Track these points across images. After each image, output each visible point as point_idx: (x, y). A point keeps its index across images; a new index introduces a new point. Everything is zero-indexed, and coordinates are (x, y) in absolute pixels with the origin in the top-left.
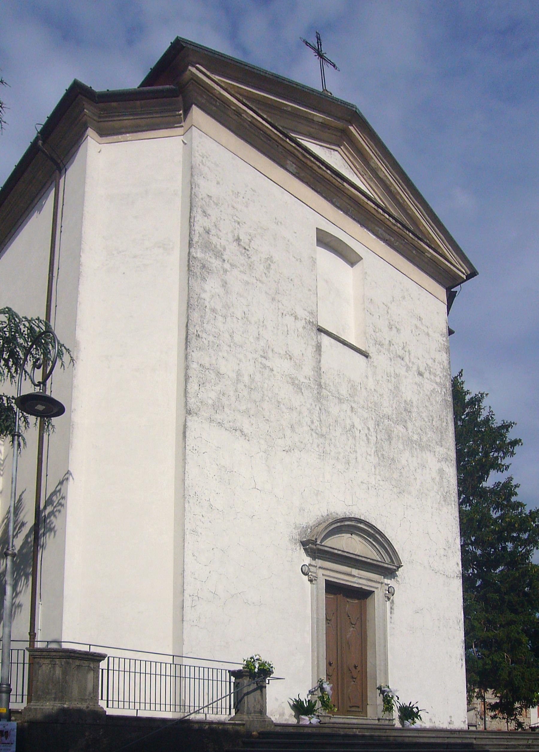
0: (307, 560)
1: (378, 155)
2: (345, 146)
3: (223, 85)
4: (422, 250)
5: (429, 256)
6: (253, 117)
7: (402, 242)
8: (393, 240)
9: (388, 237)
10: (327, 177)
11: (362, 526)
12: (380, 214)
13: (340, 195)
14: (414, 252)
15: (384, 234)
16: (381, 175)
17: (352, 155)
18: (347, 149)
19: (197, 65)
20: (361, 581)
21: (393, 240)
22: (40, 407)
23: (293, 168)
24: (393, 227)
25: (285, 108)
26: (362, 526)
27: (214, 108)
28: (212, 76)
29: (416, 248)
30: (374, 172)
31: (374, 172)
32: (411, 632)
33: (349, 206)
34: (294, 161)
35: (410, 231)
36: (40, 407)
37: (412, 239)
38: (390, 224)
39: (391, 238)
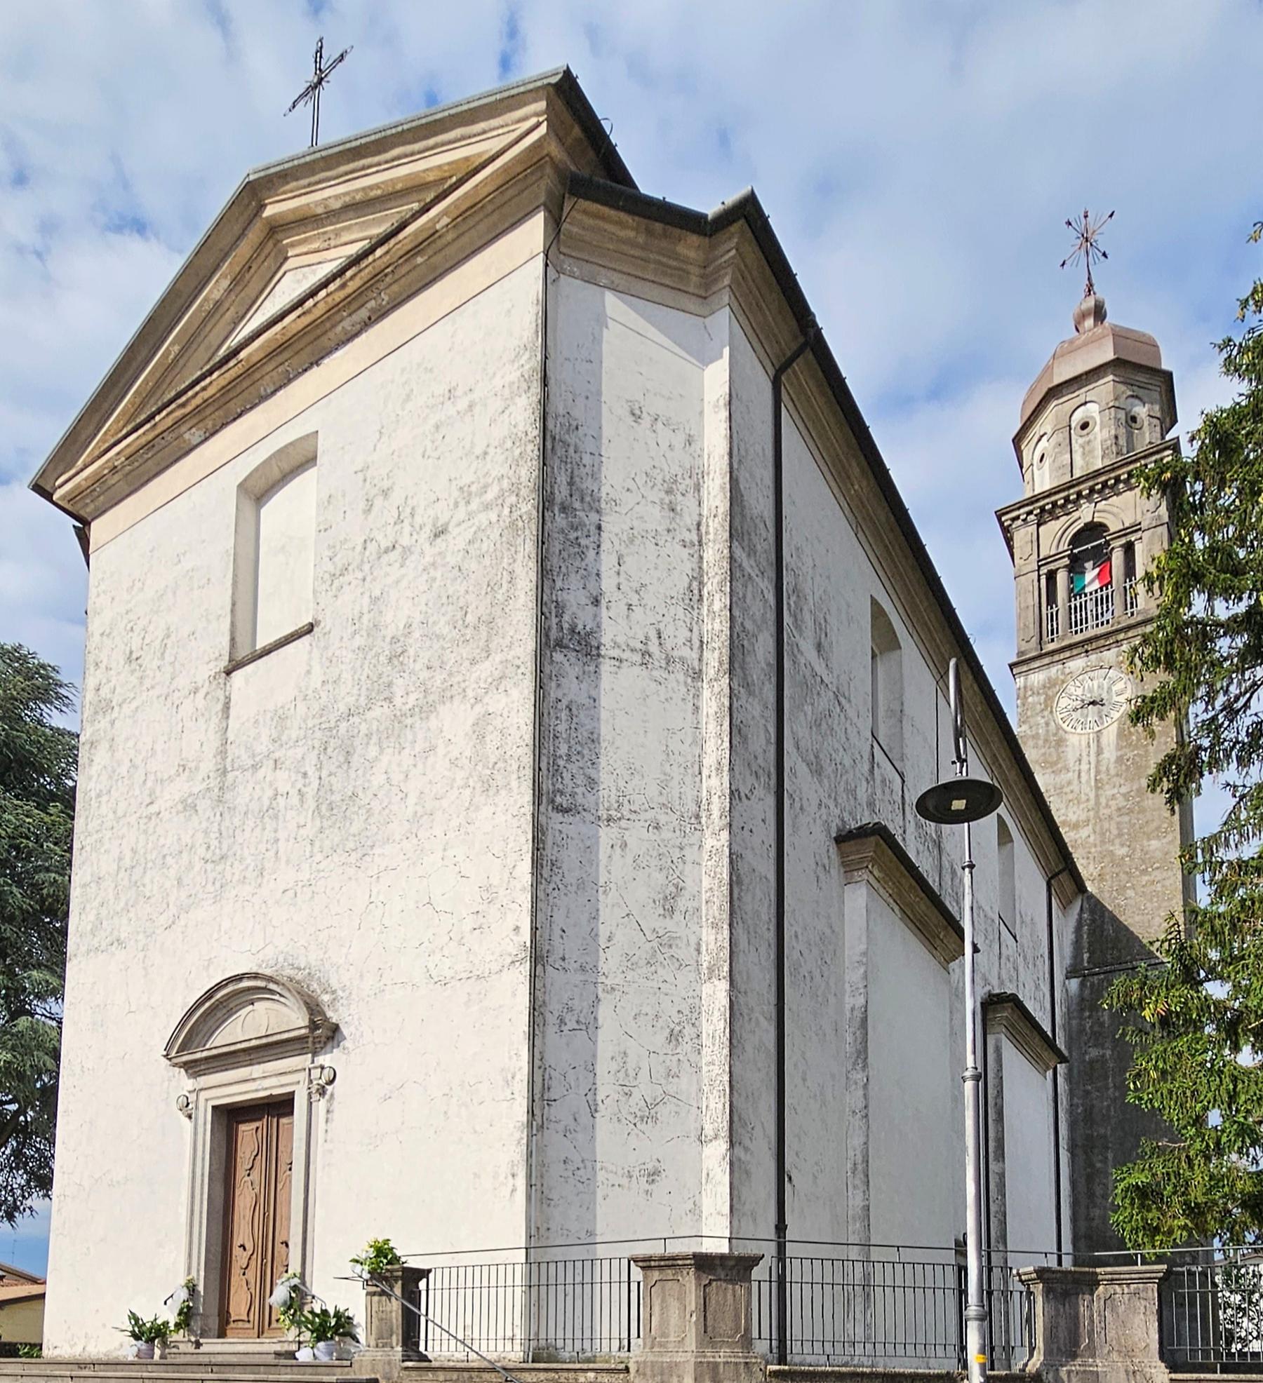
0: (186, 1083)
1: (309, 185)
2: (292, 245)
3: (97, 453)
4: (425, 235)
5: (446, 220)
6: (118, 454)
7: (388, 280)
8: (372, 304)
9: (363, 314)
10: (223, 382)
11: (246, 984)
12: (314, 310)
13: (257, 375)
14: (419, 260)
15: (355, 317)
16: (337, 205)
17: (305, 241)
18: (300, 243)
19: (57, 483)
20: (267, 1083)
21: (372, 304)
22: (959, 805)
23: (193, 436)
24: (349, 290)
25: (172, 357)
26: (246, 984)
27: (102, 498)
28: (80, 463)
29: (416, 250)
30: (332, 216)
31: (332, 216)
32: (371, 1147)
33: (280, 369)
34: (188, 425)
35: (372, 250)
36: (959, 805)
37: (387, 252)
38: (342, 294)
39: (369, 305)
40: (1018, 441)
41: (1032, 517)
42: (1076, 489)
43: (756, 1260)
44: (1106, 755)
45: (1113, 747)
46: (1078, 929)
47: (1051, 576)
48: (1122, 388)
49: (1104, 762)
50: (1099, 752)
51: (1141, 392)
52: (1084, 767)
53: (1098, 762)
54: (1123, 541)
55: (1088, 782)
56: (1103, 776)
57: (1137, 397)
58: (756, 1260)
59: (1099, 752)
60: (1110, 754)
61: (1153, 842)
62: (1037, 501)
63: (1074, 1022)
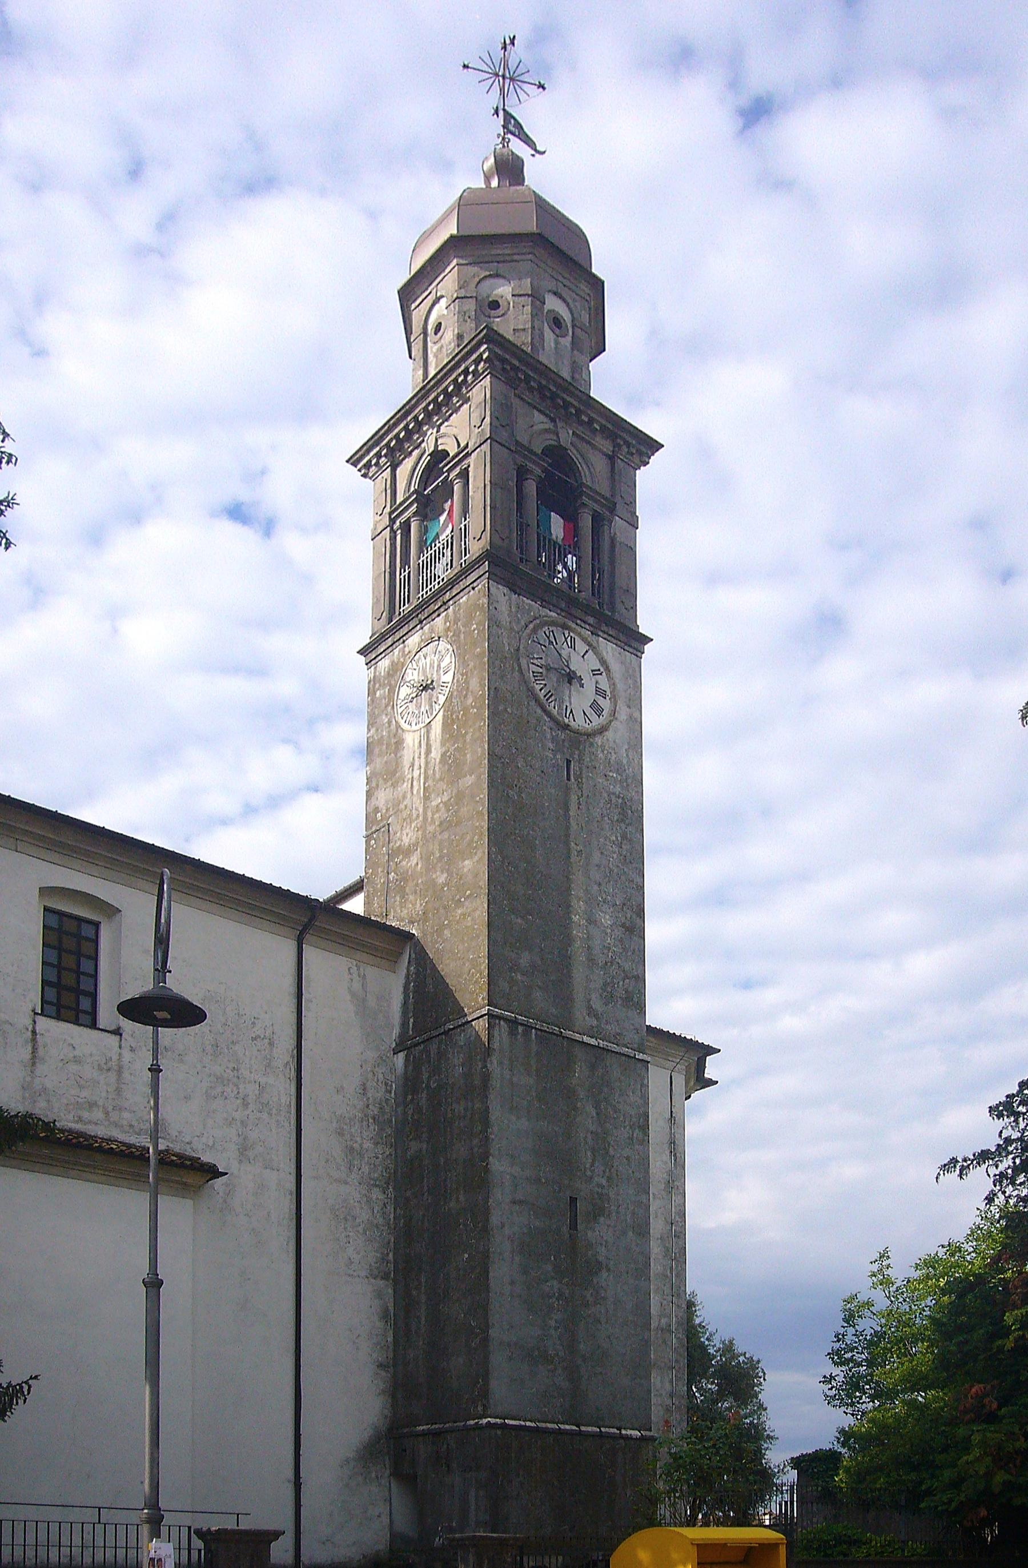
40: (410, 357)
41: (383, 460)
42: (412, 415)
43: (277, 1535)
44: (432, 755)
45: (438, 744)
46: (406, 987)
47: (406, 527)
48: (473, 270)
49: (431, 765)
50: (428, 752)
51: (503, 268)
52: (416, 773)
53: (427, 763)
54: (457, 470)
55: (418, 791)
56: (430, 782)
57: (497, 276)
58: (277, 1535)
59: (428, 752)
60: (436, 754)
61: (467, 862)
62: (382, 438)
63: (399, 1110)
